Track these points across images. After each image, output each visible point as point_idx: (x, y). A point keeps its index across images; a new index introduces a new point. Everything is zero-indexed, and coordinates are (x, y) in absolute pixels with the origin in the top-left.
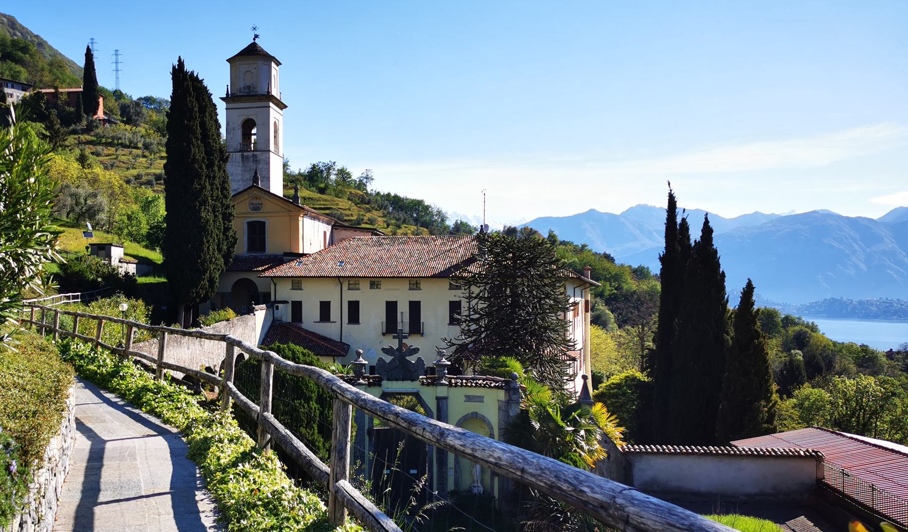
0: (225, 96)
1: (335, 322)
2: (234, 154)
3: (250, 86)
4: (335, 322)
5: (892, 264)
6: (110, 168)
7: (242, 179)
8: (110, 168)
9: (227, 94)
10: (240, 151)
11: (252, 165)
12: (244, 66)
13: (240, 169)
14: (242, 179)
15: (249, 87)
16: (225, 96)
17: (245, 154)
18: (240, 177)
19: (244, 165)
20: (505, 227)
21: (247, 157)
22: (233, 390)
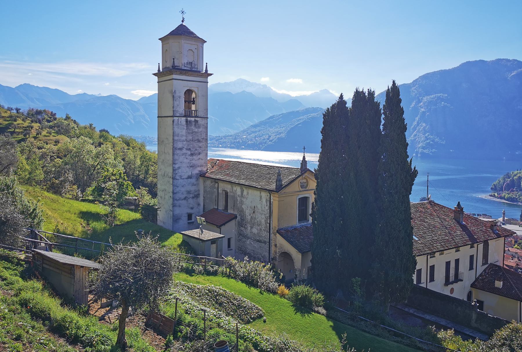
0: (157, 72)
1: (424, 283)
2: (180, 118)
3: (192, 63)
4: (424, 283)
5: (144, 121)
6: (298, 283)
7: (186, 140)
8: (298, 283)
9: (159, 70)
10: (184, 116)
11: (194, 128)
12: (174, 43)
13: (184, 131)
14: (186, 140)
15: (191, 63)
16: (157, 72)
17: (189, 119)
18: (184, 138)
19: (187, 129)
20: (100, 94)
21: (190, 122)
22: (43, 251)
